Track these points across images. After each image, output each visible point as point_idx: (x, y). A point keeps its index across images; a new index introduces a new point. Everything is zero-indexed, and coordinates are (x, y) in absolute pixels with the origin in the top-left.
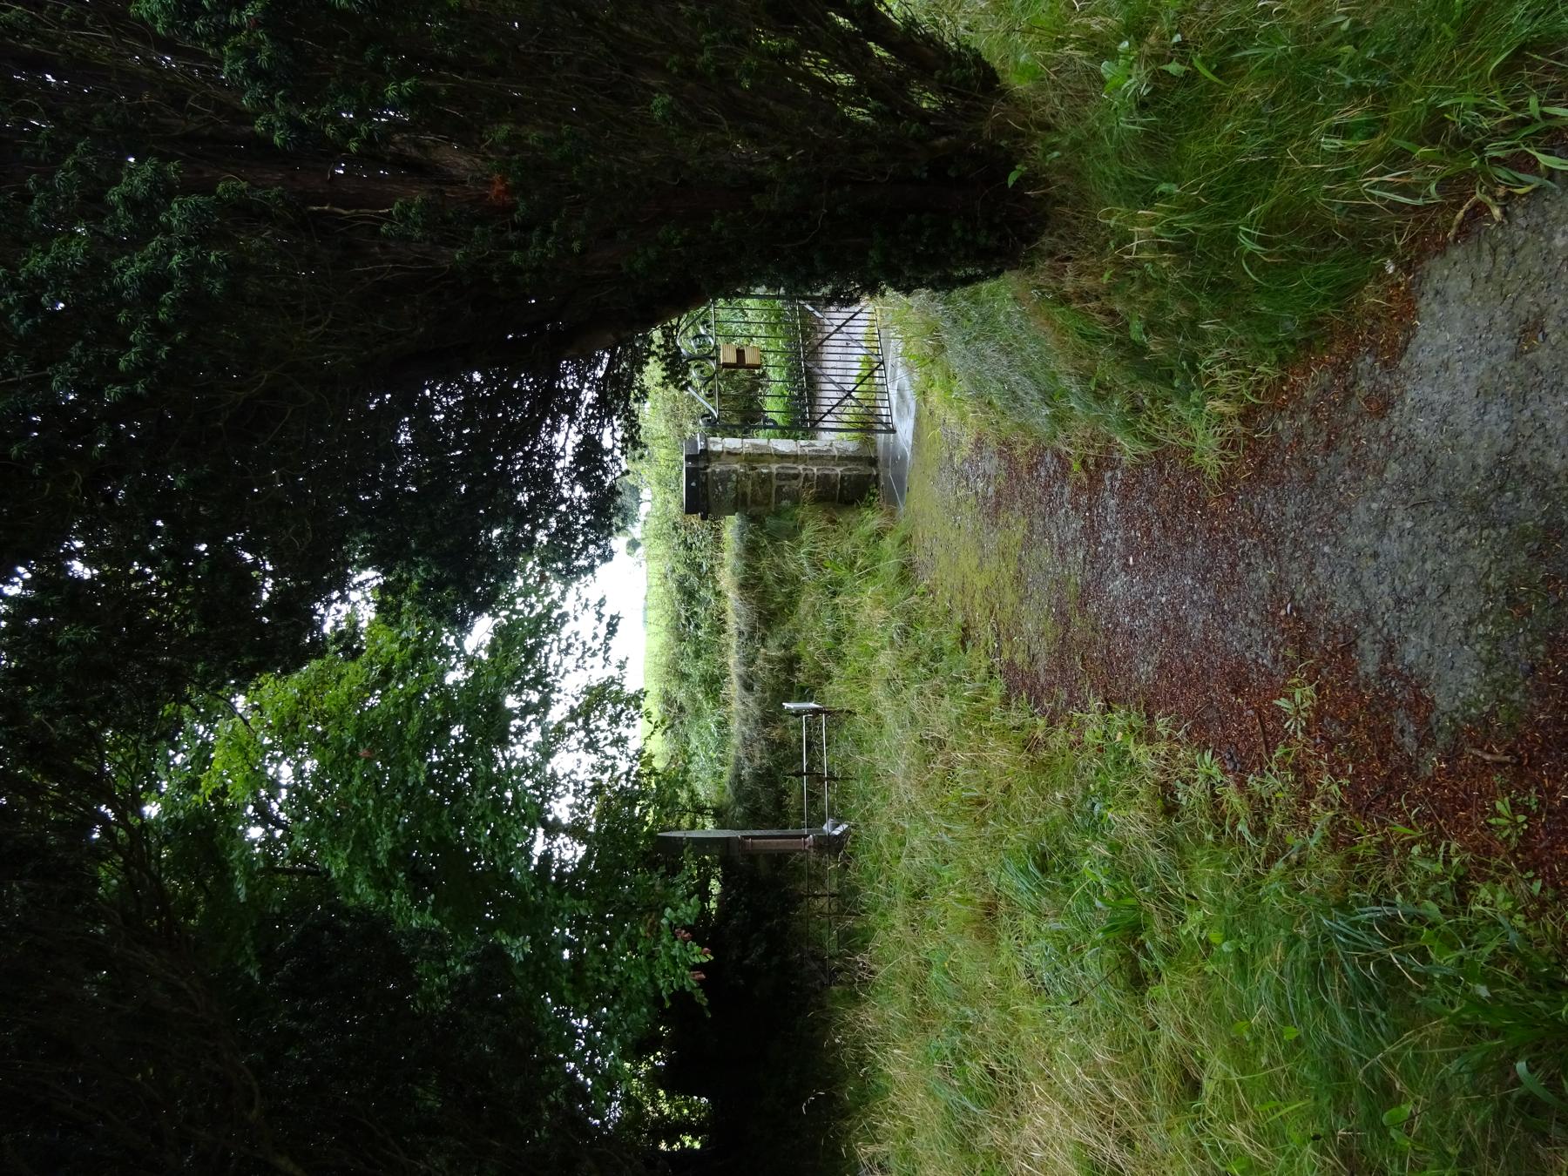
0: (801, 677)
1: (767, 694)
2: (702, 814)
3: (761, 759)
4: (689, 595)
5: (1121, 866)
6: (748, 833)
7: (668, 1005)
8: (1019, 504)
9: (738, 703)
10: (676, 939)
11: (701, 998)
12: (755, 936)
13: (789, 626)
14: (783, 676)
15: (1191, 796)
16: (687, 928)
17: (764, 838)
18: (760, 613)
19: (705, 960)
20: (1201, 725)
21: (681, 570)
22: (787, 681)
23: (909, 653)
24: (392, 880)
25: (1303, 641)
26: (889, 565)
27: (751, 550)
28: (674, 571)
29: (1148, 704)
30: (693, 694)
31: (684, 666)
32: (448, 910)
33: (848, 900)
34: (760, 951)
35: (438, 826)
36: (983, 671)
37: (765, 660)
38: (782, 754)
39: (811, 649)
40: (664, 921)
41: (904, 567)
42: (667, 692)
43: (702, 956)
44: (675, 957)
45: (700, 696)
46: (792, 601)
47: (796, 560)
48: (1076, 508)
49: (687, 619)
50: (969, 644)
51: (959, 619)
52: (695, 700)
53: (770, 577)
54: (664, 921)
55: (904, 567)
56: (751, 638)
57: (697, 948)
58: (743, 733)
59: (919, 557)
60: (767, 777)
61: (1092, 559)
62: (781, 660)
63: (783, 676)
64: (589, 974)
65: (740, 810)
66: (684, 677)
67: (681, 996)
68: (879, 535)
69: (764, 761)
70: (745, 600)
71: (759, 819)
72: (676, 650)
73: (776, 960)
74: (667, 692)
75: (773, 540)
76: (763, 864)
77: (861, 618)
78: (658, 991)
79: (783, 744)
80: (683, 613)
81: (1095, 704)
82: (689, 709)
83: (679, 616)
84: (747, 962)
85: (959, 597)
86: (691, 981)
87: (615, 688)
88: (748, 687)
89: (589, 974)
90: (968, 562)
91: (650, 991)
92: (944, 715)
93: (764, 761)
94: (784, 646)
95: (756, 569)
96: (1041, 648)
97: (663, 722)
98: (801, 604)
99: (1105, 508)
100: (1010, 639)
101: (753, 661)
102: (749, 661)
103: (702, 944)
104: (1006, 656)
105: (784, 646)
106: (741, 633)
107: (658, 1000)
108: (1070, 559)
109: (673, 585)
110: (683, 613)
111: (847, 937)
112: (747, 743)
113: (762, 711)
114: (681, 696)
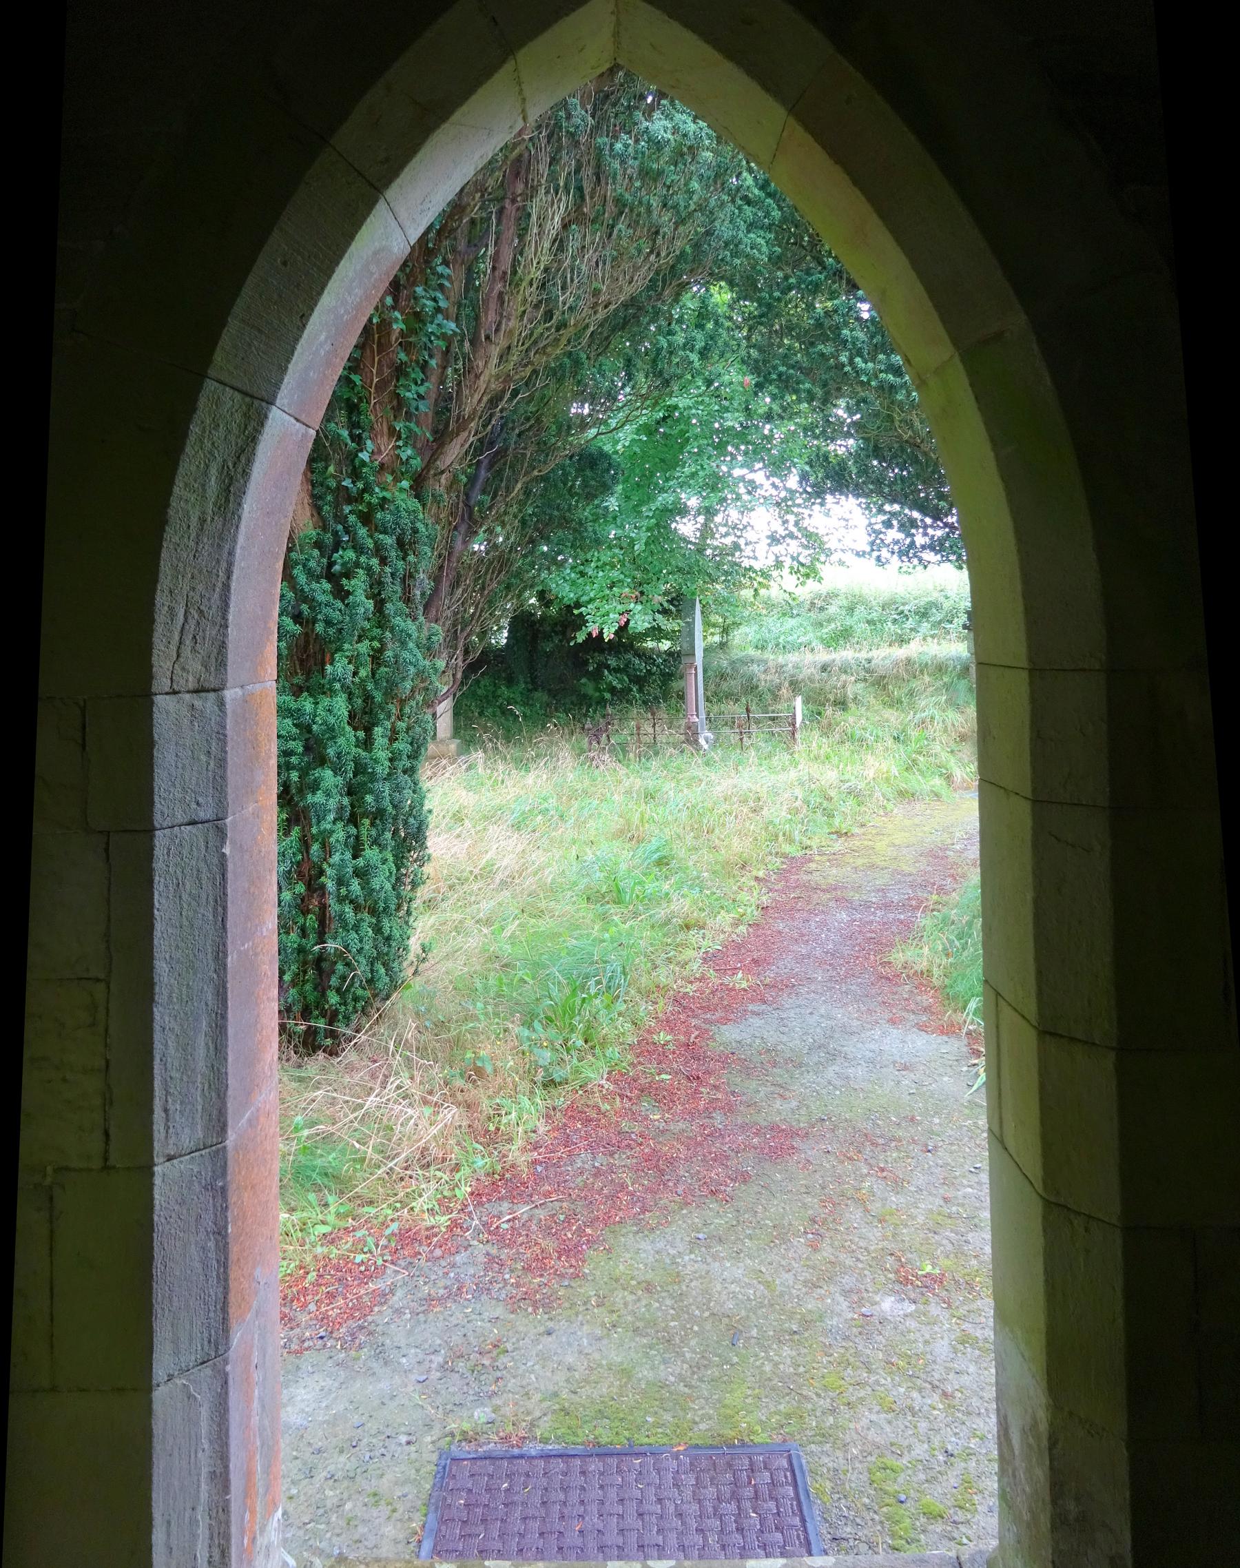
0: (829, 711)
1: (818, 685)
2: (723, 632)
3: (765, 680)
4: (923, 614)
5: (652, 900)
6: (700, 671)
7: (576, 612)
8: (929, 868)
9: (807, 661)
10: (620, 614)
11: (581, 637)
12: (626, 679)
13: (872, 701)
14: (832, 697)
15: (693, 936)
16: (628, 622)
17: (695, 684)
18: (885, 677)
19: (605, 636)
20: (739, 947)
21: (947, 605)
22: (828, 700)
23: (833, 793)
24: (657, 408)
25: (774, 986)
26: (916, 782)
27: (940, 668)
28: (947, 598)
29: (758, 925)
30: (834, 620)
31: (860, 611)
32: (638, 450)
33: (654, 749)
34: (614, 683)
35: (696, 437)
36: (809, 843)
37: (845, 682)
38: (769, 697)
39: (851, 720)
40: (632, 605)
41: (913, 795)
42: (837, 595)
43: (609, 635)
44: (608, 615)
45: (833, 625)
46: (895, 703)
47: (930, 705)
48: (909, 899)
49: (902, 612)
50: (834, 837)
51: (856, 830)
52: (829, 621)
53: (914, 684)
54: (632, 605)
55: (913, 795)
56: (868, 671)
57: (613, 630)
58: (786, 665)
59: (919, 807)
60: (751, 688)
61: (867, 905)
62: (845, 696)
63: (832, 697)
64: (596, 554)
65: (725, 663)
66: (851, 610)
67: (581, 622)
68: (949, 778)
69: (763, 683)
70: (896, 664)
71: (718, 680)
72: (874, 603)
73: (608, 696)
74: (837, 595)
75: (947, 687)
76: (681, 683)
77: (870, 759)
78: (585, 605)
79: (776, 698)
80: (907, 607)
81: (765, 900)
82: (822, 616)
83: (904, 604)
84: (606, 672)
85: (874, 832)
86: (593, 629)
87: (823, 558)
88: (824, 668)
89: (596, 554)
90: (899, 838)
91: (585, 598)
92: (777, 813)
93: (763, 683)
94: (856, 698)
95: (922, 672)
96: (816, 877)
97: (794, 599)
98: (890, 711)
99: (900, 913)
100: (829, 860)
101: (846, 672)
102: (844, 670)
103: (616, 633)
104: (817, 858)
105: (856, 698)
106: (869, 661)
107: (578, 605)
108: (873, 894)
109: (935, 596)
110: (907, 607)
111: (624, 747)
112: (780, 669)
113: (803, 680)
114: (832, 610)
